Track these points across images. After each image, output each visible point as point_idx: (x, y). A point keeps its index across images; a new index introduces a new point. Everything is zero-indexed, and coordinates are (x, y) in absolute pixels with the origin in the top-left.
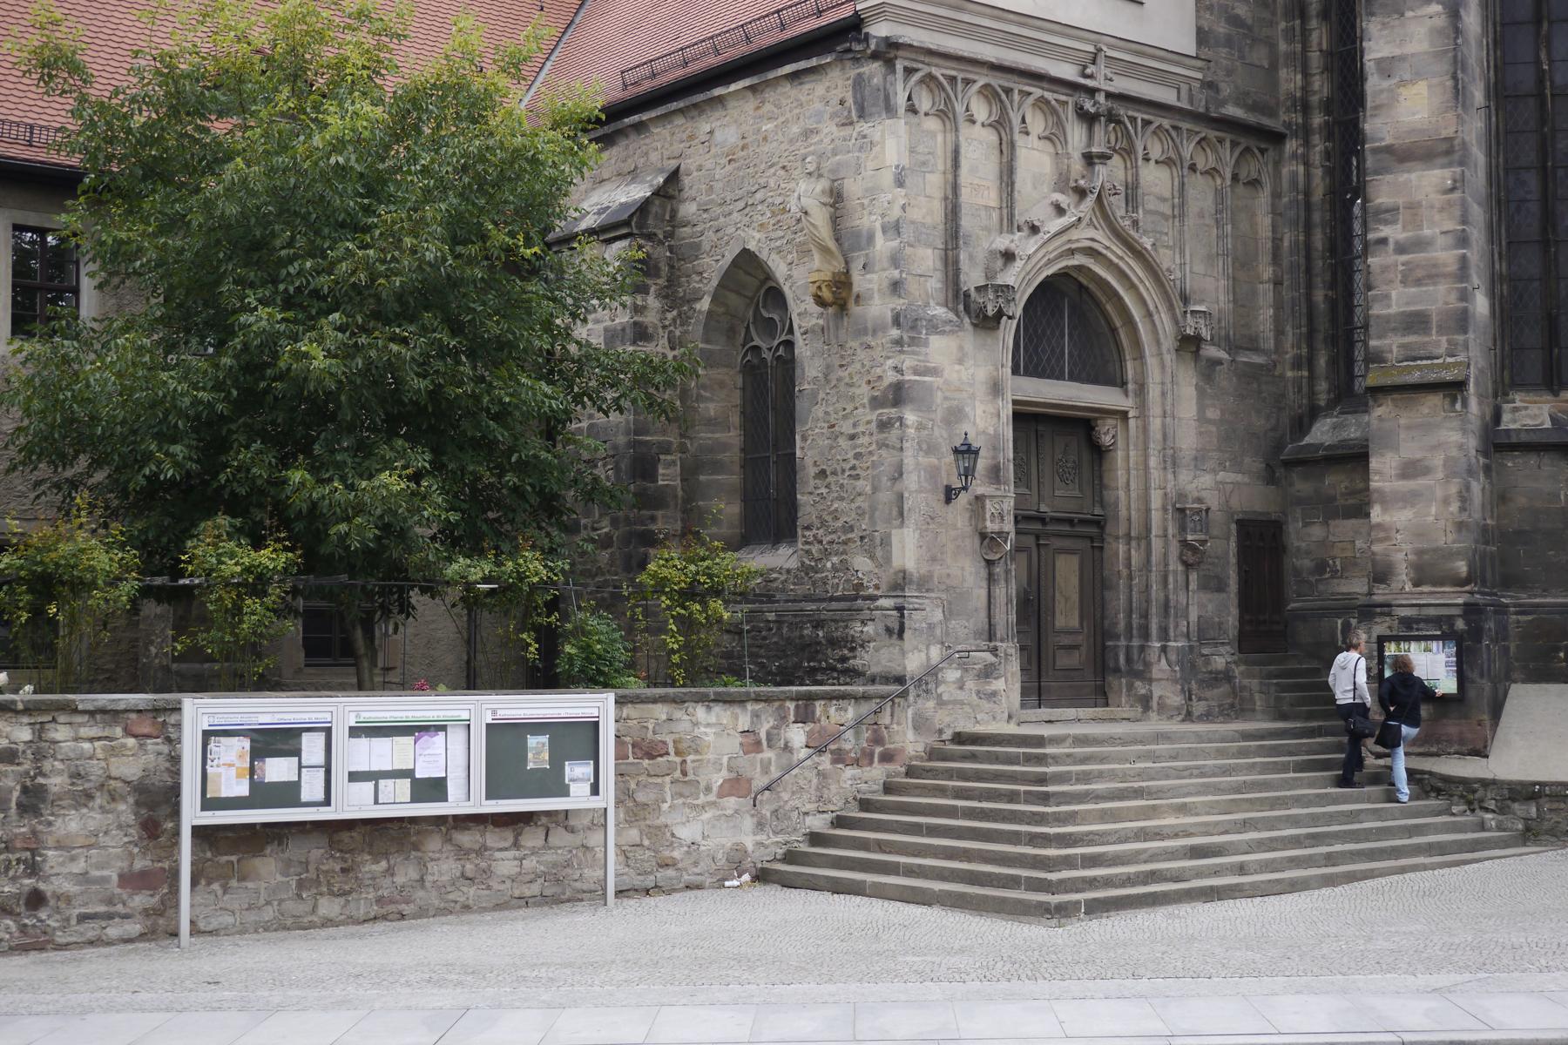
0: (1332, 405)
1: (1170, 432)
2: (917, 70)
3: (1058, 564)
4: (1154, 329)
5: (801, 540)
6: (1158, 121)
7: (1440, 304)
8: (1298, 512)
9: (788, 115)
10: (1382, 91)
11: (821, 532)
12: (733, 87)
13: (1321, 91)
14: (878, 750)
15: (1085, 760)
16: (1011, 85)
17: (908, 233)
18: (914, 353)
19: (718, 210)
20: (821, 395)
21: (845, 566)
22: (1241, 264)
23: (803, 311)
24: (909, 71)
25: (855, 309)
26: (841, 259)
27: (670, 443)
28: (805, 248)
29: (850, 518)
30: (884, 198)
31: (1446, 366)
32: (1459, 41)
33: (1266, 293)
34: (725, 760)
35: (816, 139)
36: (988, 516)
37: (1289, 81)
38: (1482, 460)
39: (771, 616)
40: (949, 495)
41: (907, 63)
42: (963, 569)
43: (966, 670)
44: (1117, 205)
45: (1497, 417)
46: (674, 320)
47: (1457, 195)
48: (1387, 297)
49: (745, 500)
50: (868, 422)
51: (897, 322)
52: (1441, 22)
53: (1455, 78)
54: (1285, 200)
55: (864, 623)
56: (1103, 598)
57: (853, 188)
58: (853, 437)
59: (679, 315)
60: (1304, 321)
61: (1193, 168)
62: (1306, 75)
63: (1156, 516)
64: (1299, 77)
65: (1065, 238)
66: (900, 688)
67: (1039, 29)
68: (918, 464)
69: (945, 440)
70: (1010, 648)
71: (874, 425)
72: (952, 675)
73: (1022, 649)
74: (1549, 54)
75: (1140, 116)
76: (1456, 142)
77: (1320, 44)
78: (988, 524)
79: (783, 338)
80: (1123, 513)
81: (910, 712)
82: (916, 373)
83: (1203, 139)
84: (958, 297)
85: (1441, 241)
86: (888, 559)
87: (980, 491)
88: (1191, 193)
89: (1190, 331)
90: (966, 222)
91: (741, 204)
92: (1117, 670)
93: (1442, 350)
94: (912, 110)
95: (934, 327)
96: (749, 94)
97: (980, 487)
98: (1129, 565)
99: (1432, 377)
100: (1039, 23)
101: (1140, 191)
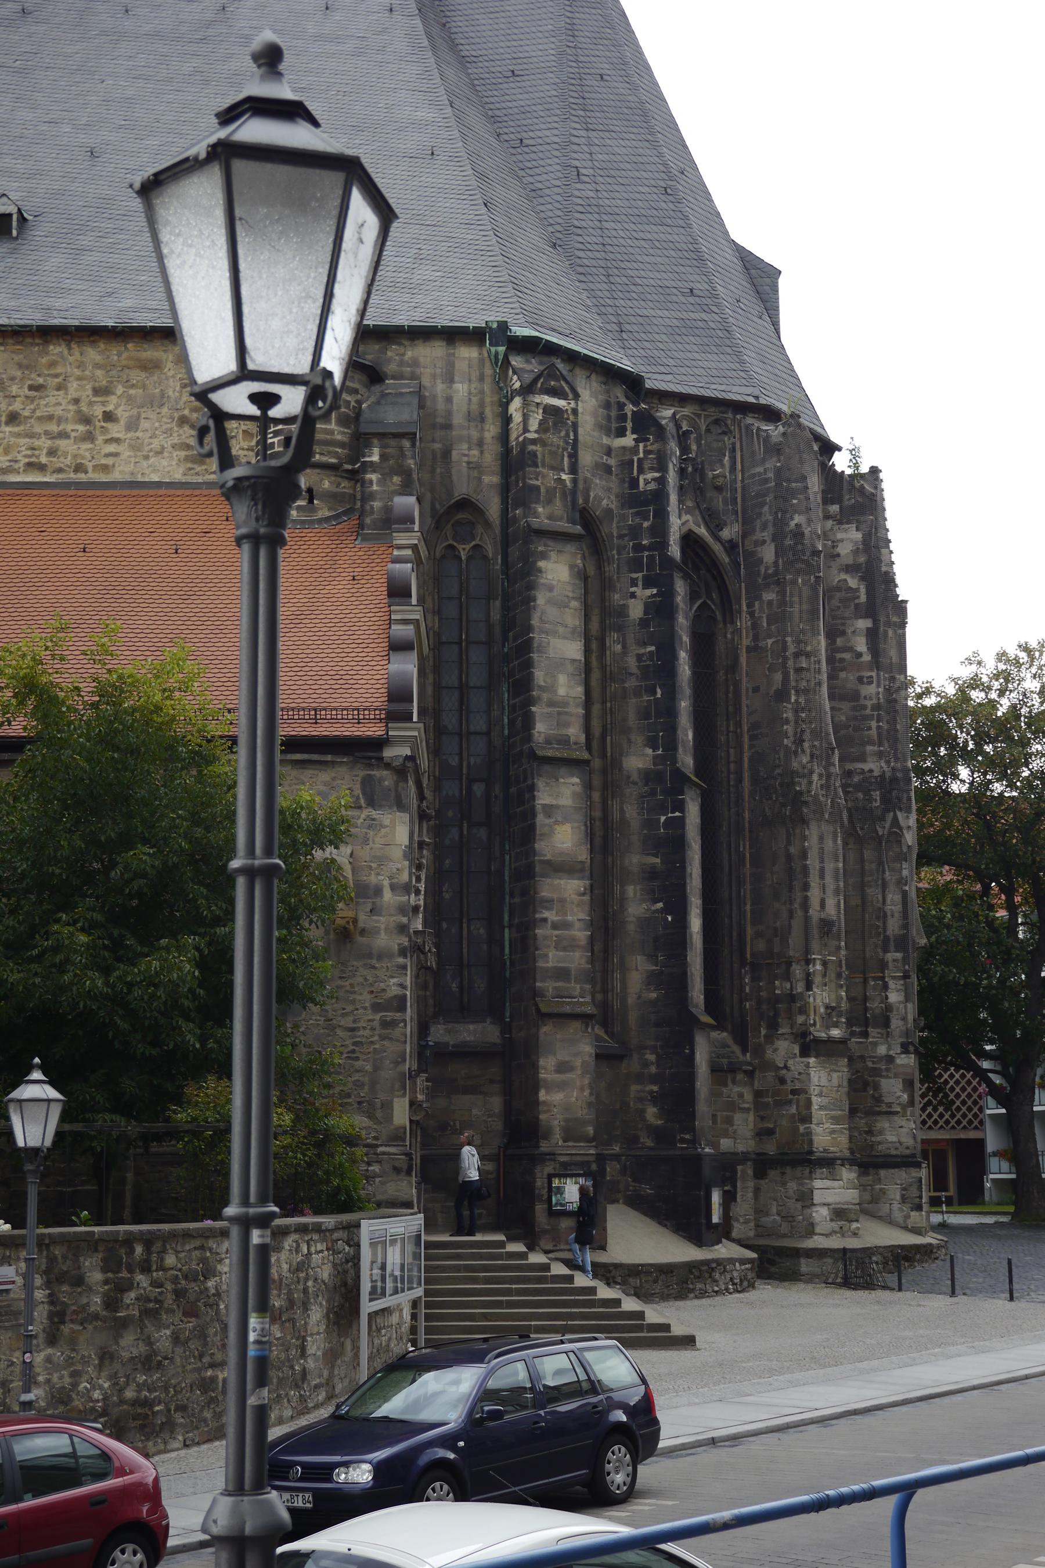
48: (546, 956)
85: (577, 925)
86: (389, 1118)
93: (577, 993)
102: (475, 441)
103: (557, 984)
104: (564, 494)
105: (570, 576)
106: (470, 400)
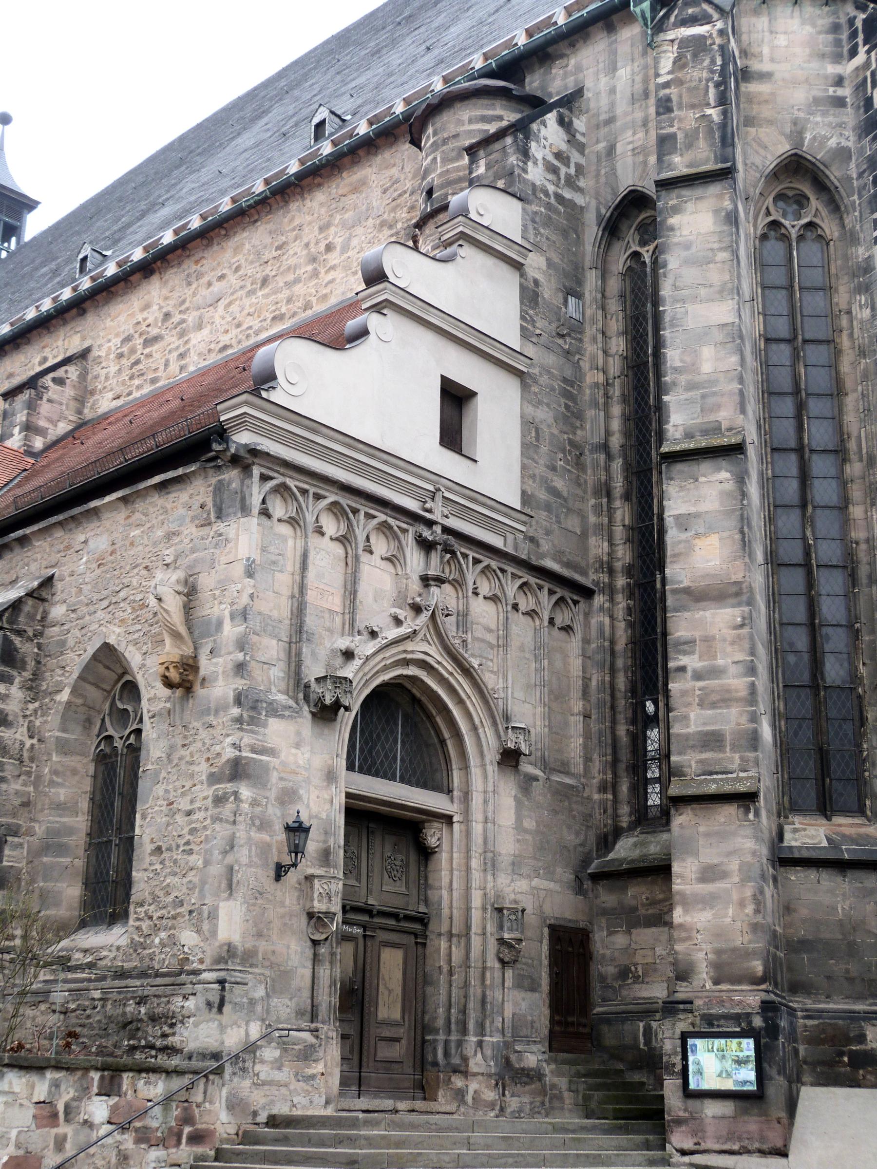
0: (632, 827)
1: (490, 836)
2: (272, 478)
3: (383, 956)
4: (481, 744)
5: (132, 916)
6: (486, 561)
7: (733, 725)
8: (603, 922)
9: (154, 521)
10: (680, 542)
11: (152, 908)
12: (108, 499)
13: (624, 558)
14: (187, 1130)
15: (399, 1144)
16: (358, 506)
17: (254, 622)
18: (253, 732)
19: (85, 610)
20: (164, 774)
21: (173, 941)
22: (555, 697)
23: (154, 695)
24: (264, 478)
25: (200, 691)
26: (191, 644)
27: (19, 826)
28: (159, 638)
29: (181, 892)
30: (233, 588)
31: (739, 780)
32: (745, 502)
33: (576, 724)
34: (14, 1134)
35: (176, 540)
36: (316, 895)
37: (598, 547)
38: (771, 870)
39: (97, 994)
40: (280, 872)
41: (264, 471)
42: (288, 947)
43: (286, 1050)
44: (449, 625)
45: (781, 836)
46: (36, 711)
47: (745, 631)
48: (686, 717)
49: (86, 884)
50: (205, 798)
51: (238, 701)
52: (730, 486)
53: (742, 532)
54: (594, 646)
55: (185, 998)
56: (424, 992)
57: (206, 581)
58: (189, 813)
59: (41, 707)
60: (609, 751)
61: (515, 607)
62: (611, 544)
63: (476, 916)
64: (606, 544)
65: (401, 648)
66: (216, 1065)
67: (386, 462)
68: (250, 838)
69: (278, 817)
70: (330, 1030)
71: (210, 800)
72: (270, 1053)
73: (344, 1037)
74: (813, 533)
75: (471, 554)
76: (744, 586)
77: (623, 520)
78: (316, 904)
79: (135, 727)
80: (445, 911)
81: (224, 1091)
82: (253, 750)
83: (525, 584)
84: (299, 686)
85: (733, 670)
86: (214, 933)
87: (310, 871)
88: (514, 629)
89: (511, 745)
90: (310, 621)
91: (105, 603)
92: (435, 1064)
93: (735, 766)
94: (265, 513)
95: (274, 711)
96: (121, 505)
97: (308, 866)
98: (450, 961)
99: (728, 788)
100: (385, 457)
101: (469, 618)
102: (640, 123)
103: (704, 756)
104: (710, 131)
105: (715, 223)
106: (633, 81)
